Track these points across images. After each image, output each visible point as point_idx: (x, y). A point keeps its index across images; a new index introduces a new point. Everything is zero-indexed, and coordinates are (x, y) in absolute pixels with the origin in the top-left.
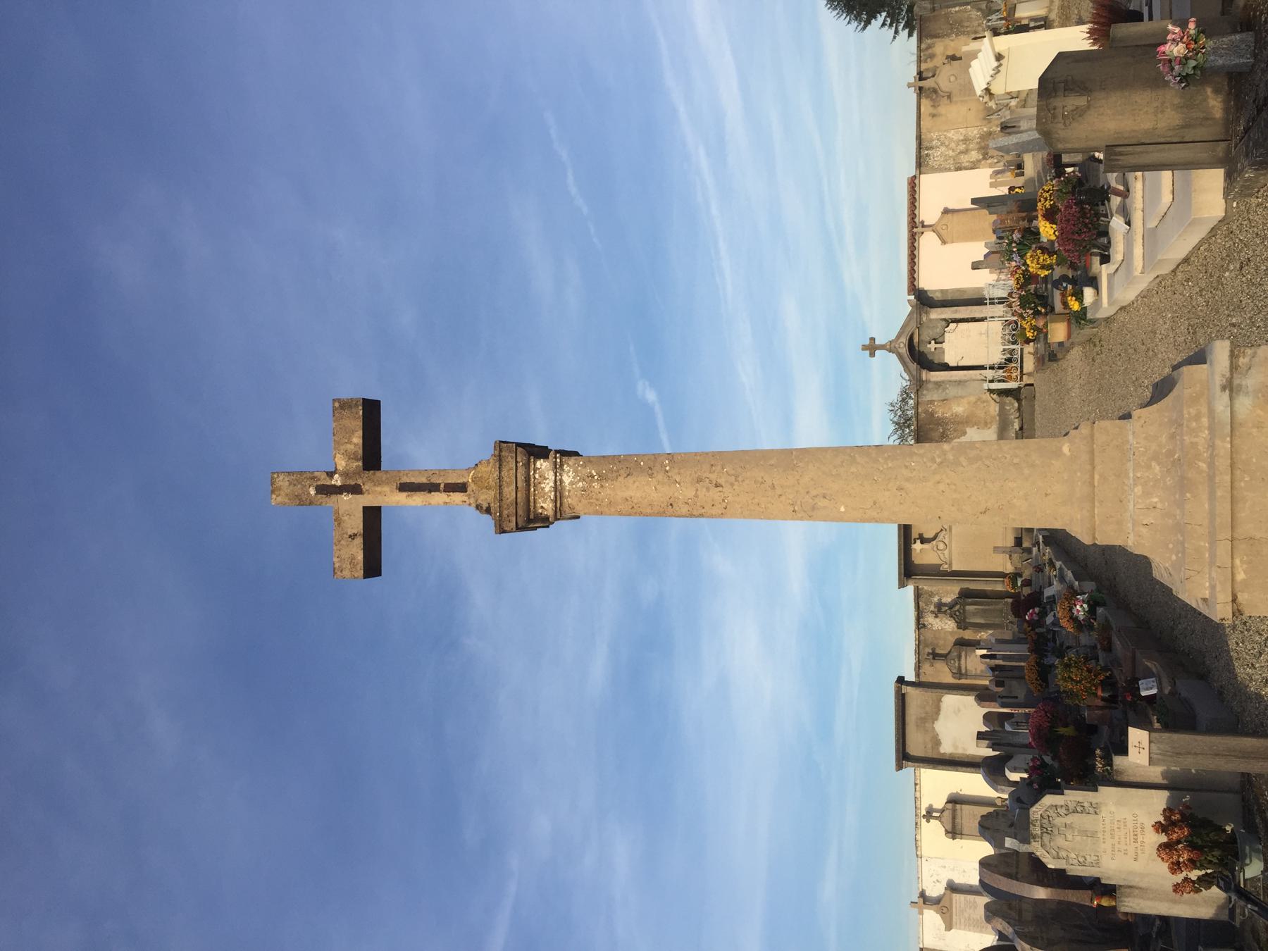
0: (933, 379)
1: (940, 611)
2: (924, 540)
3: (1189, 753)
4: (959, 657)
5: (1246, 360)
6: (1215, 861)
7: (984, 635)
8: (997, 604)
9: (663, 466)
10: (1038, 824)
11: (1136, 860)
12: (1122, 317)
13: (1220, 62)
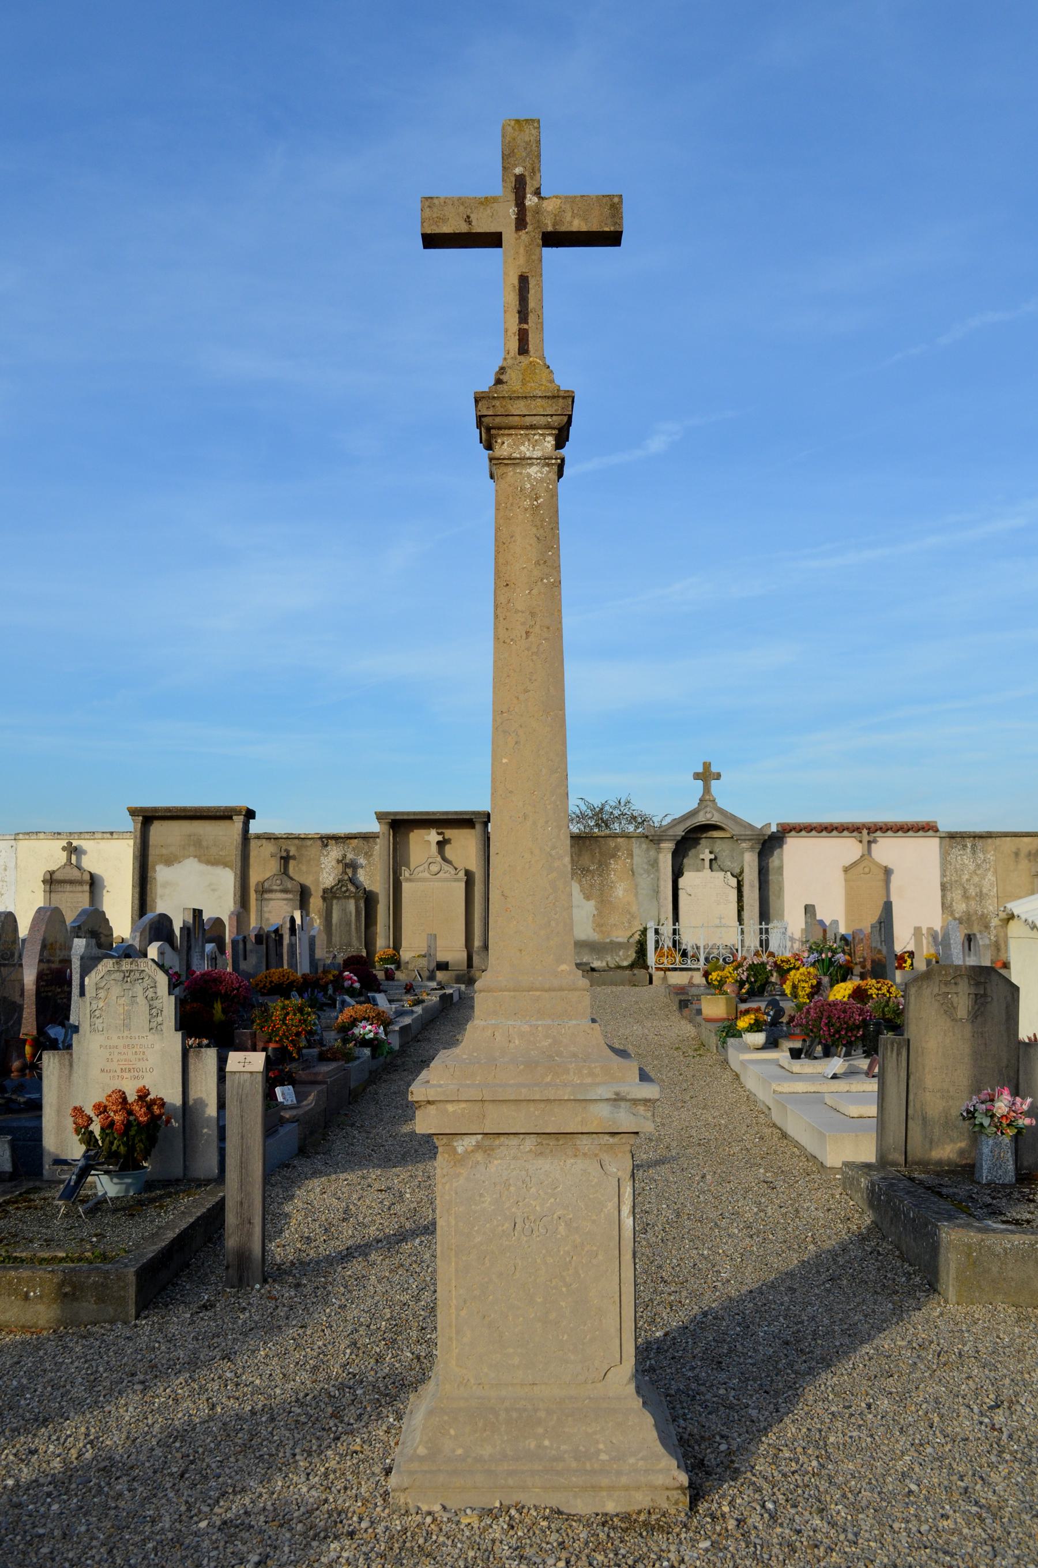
0: (661, 856)
1: (346, 866)
2: (442, 844)
3: (242, 1111)
4: (285, 891)
5: (642, 1112)
6: (114, 1148)
8: (359, 938)
10: (134, 967)
11: (102, 1071)
12: (728, 1076)
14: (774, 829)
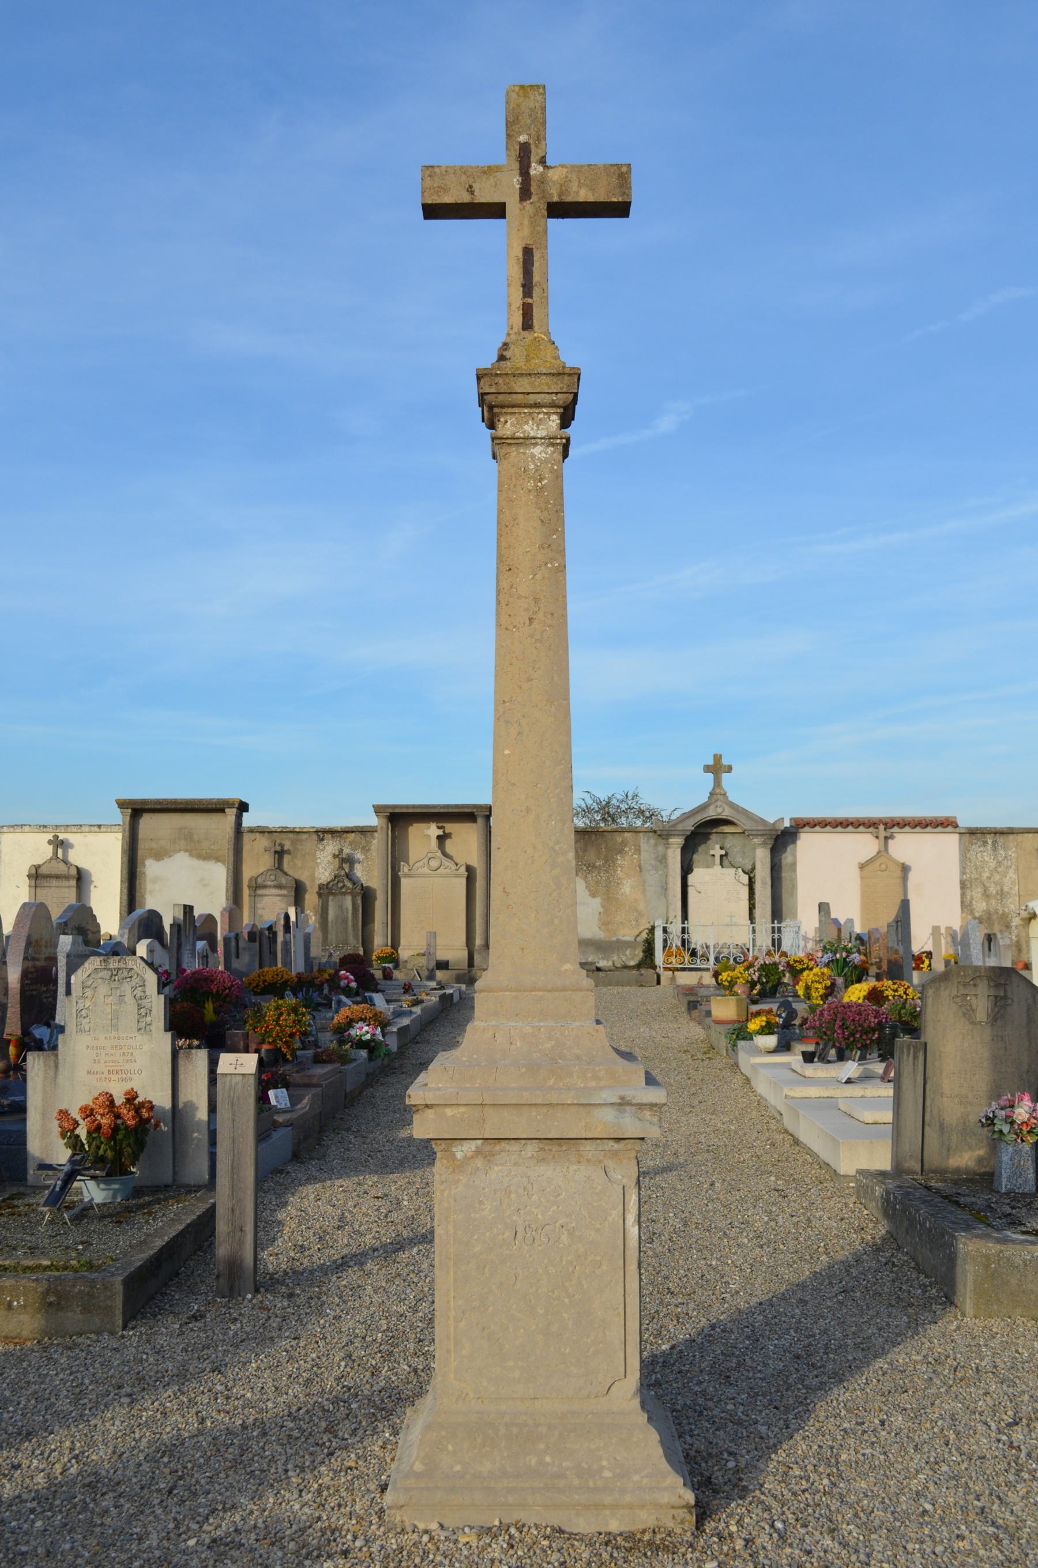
0: (670, 852)
1: (343, 861)
2: (442, 839)
4: (279, 887)
5: (648, 1118)
6: (101, 1152)
7: (312, 919)
8: (356, 937)
9: (552, 560)
10: (122, 965)
11: (89, 1072)
12: (738, 1080)
13: (1005, 1158)
14: (787, 824)
